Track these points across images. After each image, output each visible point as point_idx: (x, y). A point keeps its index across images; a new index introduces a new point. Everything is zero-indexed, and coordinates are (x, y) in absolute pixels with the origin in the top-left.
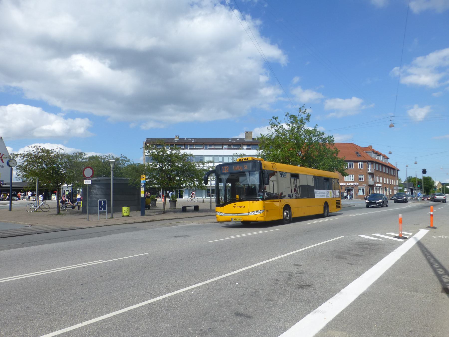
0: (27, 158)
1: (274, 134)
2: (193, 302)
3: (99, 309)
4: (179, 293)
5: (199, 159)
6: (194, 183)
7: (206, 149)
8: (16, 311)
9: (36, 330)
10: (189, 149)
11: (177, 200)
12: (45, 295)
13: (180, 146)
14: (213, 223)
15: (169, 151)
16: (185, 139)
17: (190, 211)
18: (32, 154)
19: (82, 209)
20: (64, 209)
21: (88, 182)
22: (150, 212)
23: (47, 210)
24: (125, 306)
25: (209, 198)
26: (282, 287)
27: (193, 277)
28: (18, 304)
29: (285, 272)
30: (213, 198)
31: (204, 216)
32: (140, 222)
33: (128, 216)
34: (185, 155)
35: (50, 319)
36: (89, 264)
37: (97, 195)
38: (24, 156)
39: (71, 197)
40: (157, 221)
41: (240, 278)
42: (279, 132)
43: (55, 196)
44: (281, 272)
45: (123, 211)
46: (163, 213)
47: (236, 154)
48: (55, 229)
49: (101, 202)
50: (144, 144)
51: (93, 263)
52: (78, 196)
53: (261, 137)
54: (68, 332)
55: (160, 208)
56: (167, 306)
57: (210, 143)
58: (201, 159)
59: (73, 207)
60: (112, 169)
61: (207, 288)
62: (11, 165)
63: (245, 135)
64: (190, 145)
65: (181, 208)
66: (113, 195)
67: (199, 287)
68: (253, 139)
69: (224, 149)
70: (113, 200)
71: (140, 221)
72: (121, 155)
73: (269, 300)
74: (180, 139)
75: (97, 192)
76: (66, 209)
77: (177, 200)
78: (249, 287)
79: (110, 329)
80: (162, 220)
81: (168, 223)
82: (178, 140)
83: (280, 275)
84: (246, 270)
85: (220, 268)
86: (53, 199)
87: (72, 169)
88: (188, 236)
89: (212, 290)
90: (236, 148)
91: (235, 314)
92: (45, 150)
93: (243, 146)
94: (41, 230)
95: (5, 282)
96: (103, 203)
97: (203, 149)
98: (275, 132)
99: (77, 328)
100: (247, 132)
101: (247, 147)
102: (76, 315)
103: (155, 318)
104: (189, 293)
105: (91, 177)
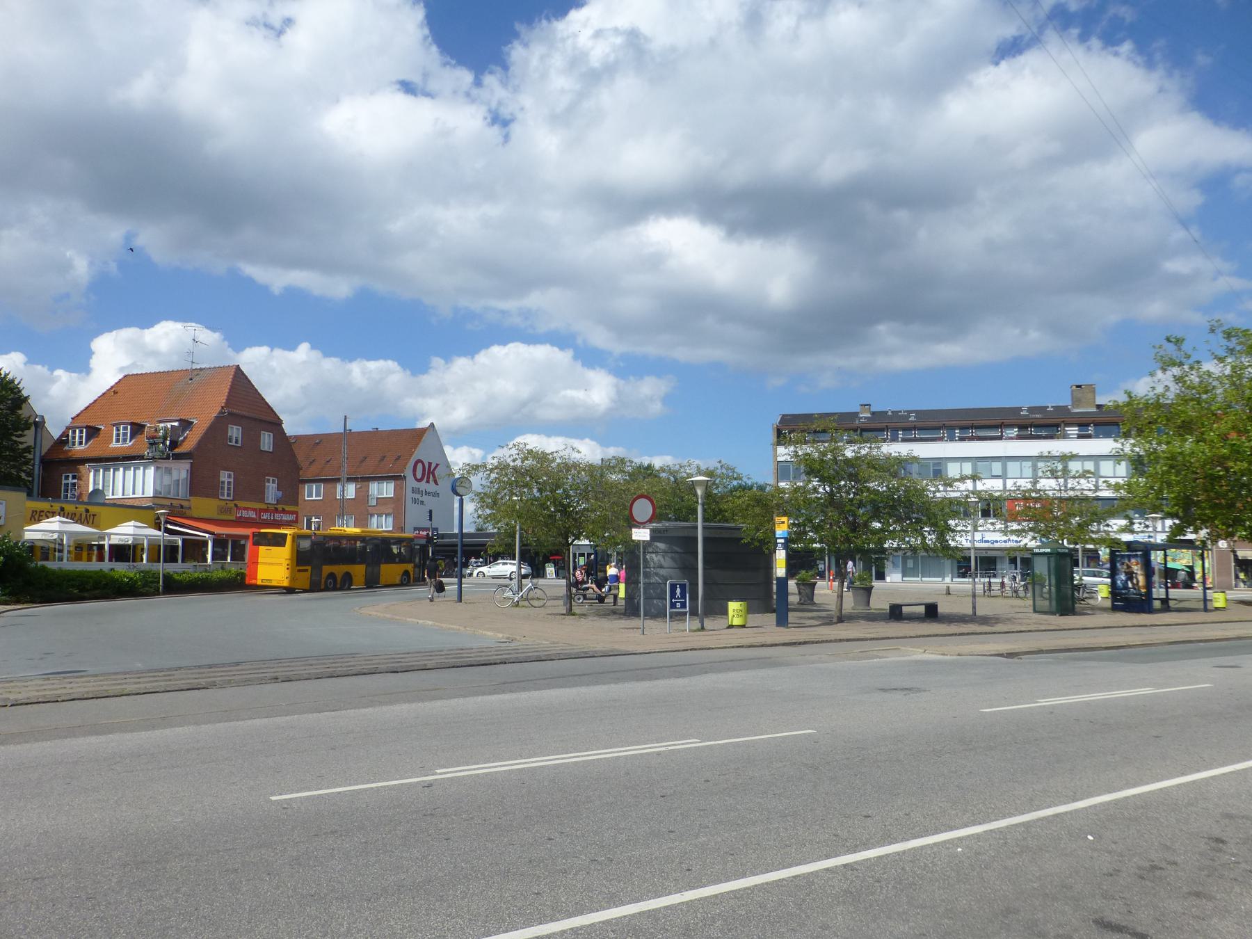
0: (497, 473)
1: (1172, 389)
2: (965, 874)
3: (718, 862)
4: (922, 848)
5: (932, 468)
6: (924, 538)
7: (952, 439)
8: (525, 845)
9: (577, 896)
10: (900, 440)
11: (872, 587)
12: (582, 815)
13: (876, 433)
14: (986, 655)
15: (852, 448)
16: (890, 413)
17: (912, 618)
18: (509, 465)
19: (624, 604)
20: (581, 601)
21: (641, 535)
22: (801, 618)
23: (541, 603)
24: (780, 863)
25: (969, 583)
26: (1239, 863)
27: (954, 807)
28: (525, 828)
29: (1243, 817)
30: (996, 583)
31: (956, 635)
32: (776, 645)
33: (743, 626)
34: (902, 462)
35: (605, 874)
36: (669, 746)
37: (661, 567)
38: (491, 470)
39: (595, 568)
40: (822, 642)
41: (1098, 823)
42: (1189, 382)
43: (553, 569)
44: (1230, 816)
45: (731, 613)
46: (836, 623)
47: (1049, 453)
48: (568, 651)
49: (673, 587)
50: (773, 429)
51: (679, 744)
52: (612, 571)
53: (1127, 399)
54: (653, 910)
55: (827, 606)
56: (895, 879)
57: (962, 422)
58: (937, 468)
59: (601, 599)
60: (700, 501)
61: (1002, 841)
62: (460, 490)
63: (1072, 394)
64: (904, 429)
65: (884, 609)
66: (704, 569)
67: (977, 837)
68: (1099, 407)
69: (1006, 439)
70: (705, 583)
71: (778, 643)
72: (720, 462)
73: (1198, 895)
74: (873, 413)
75: (661, 563)
76: (584, 601)
77: (872, 587)
78: (1131, 853)
79: (754, 917)
80: (836, 641)
81: (855, 651)
82: (869, 415)
83: (1226, 826)
84: (1114, 800)
85: (1031, 789)
86: (548, 577)
87: (600, 501)
88: (919, 690)
89: (1017, 850)
90: (1044, 434)
91: (1096, 922)
92: (538, 454)
93: (1066, 429)
94: (536, 654)
95: (486, 774)
96: (678, 590)
97: (941, 439)
98: (1174, 383)
99: (672, 905)
100: (1078, 386)
101: (1079, 430)
102: (663, 872)
103: (868, 905)
104: (948, 848)
105: (650, 521)
